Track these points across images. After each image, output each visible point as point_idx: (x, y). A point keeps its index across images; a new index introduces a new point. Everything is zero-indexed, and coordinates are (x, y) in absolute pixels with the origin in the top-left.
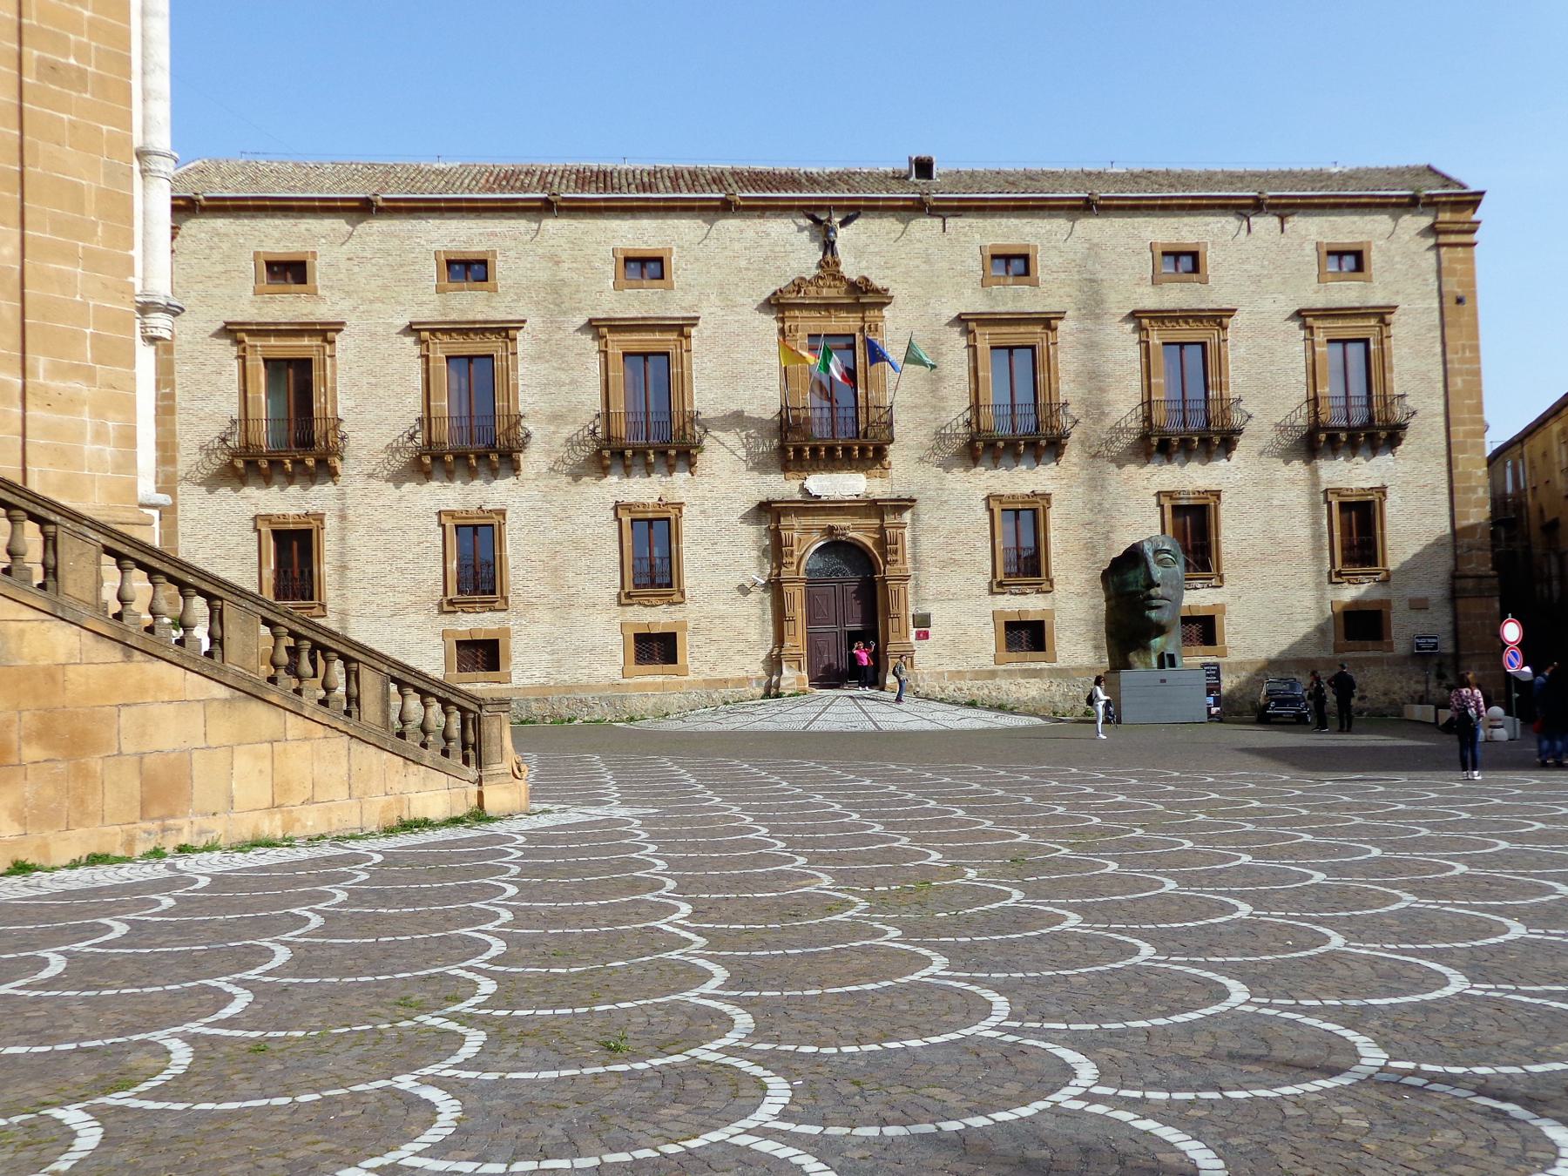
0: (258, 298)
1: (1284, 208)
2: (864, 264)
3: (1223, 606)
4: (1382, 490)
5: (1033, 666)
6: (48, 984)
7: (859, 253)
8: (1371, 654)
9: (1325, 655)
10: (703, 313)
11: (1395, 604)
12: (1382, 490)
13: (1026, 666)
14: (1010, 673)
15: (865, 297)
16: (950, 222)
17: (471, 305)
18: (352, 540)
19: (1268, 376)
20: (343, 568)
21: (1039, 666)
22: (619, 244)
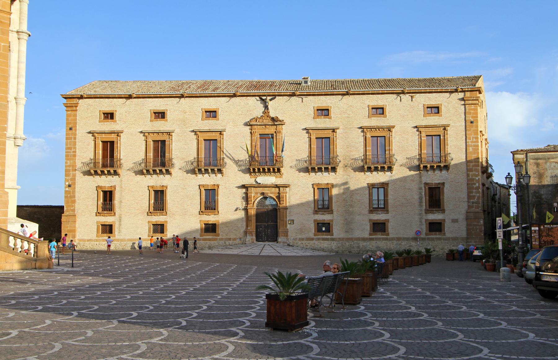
4: (443, 184)
5: (326, 237)
8: (438, 236)
12: (443, 184)
14: (319, 239)
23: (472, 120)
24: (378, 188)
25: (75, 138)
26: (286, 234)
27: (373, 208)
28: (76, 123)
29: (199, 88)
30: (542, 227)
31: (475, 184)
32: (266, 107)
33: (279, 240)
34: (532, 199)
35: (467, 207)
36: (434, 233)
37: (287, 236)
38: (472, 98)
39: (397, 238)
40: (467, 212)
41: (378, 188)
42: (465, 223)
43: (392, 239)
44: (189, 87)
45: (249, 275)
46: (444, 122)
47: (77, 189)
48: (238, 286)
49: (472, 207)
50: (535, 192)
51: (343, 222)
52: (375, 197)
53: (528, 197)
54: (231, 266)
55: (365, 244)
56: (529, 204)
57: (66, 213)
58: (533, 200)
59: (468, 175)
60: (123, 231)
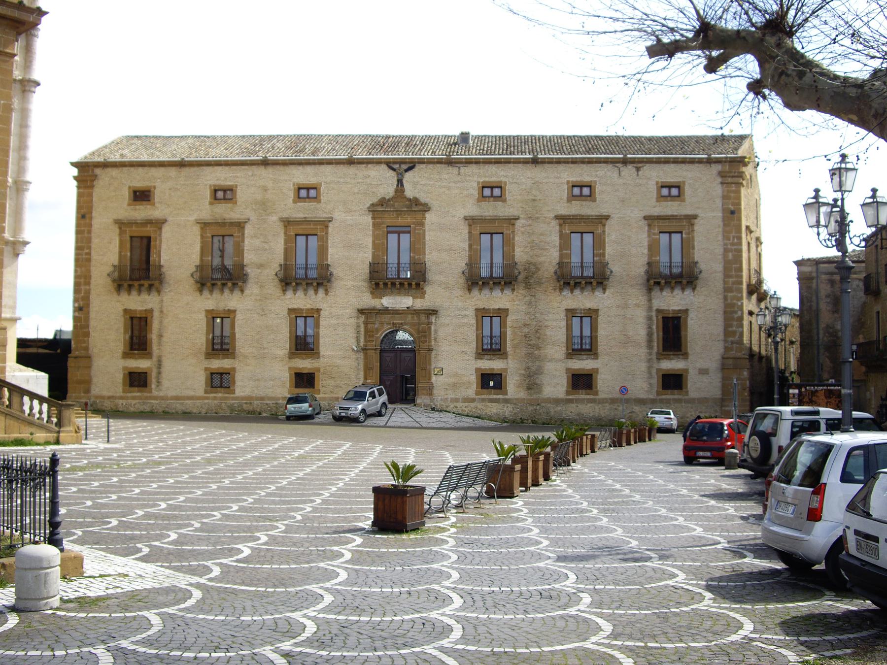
0: (129, 208)
1: (638, 164)
2: (416, 191)
3: (597, 369)
4: (686, 311)
5: (495, 396)
6: (111, 529)
7: (415, 185)
8: (676, 397)
9: (651, 397)
10: (335, 215)
11: (691, 371)
12: (686, 311)
13: (492, 396)
14: (483, 400)
15: (419, 207)
16: (463, 169)
17: (224, 212)
18: (166, 322)
19: (628, 248)
20: (160, 336)
21: (498, 397)
22: (296, 181)
23: (732, 208)
24: (581, 317)
25: (90, 232)
26: (430, 390)
27: (573, 350)
28: (92, 207)
29: (288, 148)
30: (803, 390)
31: (736, 312)
32: (400, 182)
33: (419, 401)
34: (823, 337)
35: (722, 350)
36: (669, 391)
37: (431, 394)
38: (733, 174)
39: (610, 399)
40: (723, 358)
41: (581, 317)
42: (720, 375)
43: (603, 401)
44: (273, 148)
45: (371, 458)
46: (688, 211)
47: (92, 315)
48: (357, 475)
49: (732, 349)
50: (828, 326)
51: (523, 372)
52: (576, 332)
53: (818, 334)
54: (342, 445)
55: (559, 408)
56: (818, 346)
57: (75, 353)
58: (825, 339)
59: (725, 298)
60: (165, 383)
